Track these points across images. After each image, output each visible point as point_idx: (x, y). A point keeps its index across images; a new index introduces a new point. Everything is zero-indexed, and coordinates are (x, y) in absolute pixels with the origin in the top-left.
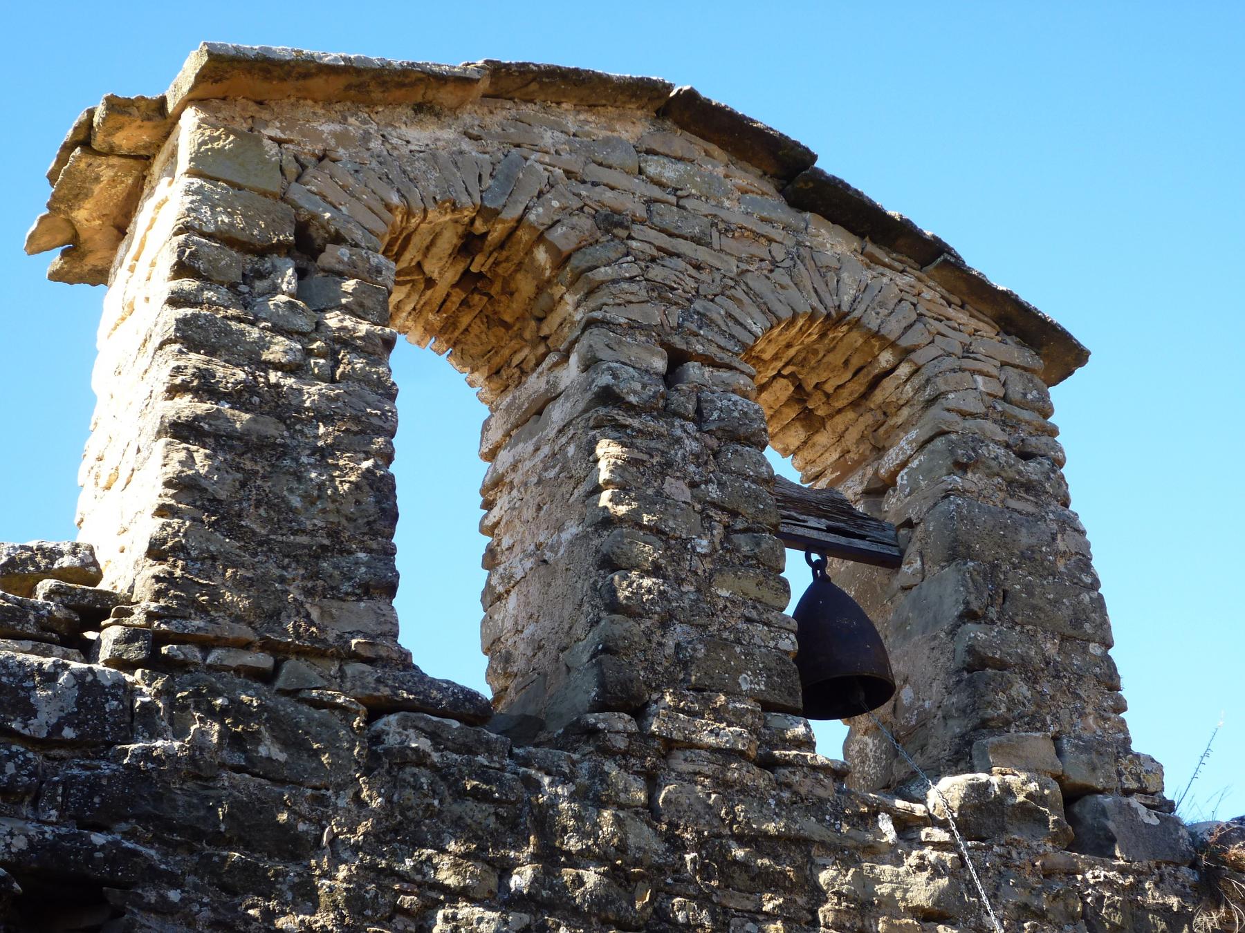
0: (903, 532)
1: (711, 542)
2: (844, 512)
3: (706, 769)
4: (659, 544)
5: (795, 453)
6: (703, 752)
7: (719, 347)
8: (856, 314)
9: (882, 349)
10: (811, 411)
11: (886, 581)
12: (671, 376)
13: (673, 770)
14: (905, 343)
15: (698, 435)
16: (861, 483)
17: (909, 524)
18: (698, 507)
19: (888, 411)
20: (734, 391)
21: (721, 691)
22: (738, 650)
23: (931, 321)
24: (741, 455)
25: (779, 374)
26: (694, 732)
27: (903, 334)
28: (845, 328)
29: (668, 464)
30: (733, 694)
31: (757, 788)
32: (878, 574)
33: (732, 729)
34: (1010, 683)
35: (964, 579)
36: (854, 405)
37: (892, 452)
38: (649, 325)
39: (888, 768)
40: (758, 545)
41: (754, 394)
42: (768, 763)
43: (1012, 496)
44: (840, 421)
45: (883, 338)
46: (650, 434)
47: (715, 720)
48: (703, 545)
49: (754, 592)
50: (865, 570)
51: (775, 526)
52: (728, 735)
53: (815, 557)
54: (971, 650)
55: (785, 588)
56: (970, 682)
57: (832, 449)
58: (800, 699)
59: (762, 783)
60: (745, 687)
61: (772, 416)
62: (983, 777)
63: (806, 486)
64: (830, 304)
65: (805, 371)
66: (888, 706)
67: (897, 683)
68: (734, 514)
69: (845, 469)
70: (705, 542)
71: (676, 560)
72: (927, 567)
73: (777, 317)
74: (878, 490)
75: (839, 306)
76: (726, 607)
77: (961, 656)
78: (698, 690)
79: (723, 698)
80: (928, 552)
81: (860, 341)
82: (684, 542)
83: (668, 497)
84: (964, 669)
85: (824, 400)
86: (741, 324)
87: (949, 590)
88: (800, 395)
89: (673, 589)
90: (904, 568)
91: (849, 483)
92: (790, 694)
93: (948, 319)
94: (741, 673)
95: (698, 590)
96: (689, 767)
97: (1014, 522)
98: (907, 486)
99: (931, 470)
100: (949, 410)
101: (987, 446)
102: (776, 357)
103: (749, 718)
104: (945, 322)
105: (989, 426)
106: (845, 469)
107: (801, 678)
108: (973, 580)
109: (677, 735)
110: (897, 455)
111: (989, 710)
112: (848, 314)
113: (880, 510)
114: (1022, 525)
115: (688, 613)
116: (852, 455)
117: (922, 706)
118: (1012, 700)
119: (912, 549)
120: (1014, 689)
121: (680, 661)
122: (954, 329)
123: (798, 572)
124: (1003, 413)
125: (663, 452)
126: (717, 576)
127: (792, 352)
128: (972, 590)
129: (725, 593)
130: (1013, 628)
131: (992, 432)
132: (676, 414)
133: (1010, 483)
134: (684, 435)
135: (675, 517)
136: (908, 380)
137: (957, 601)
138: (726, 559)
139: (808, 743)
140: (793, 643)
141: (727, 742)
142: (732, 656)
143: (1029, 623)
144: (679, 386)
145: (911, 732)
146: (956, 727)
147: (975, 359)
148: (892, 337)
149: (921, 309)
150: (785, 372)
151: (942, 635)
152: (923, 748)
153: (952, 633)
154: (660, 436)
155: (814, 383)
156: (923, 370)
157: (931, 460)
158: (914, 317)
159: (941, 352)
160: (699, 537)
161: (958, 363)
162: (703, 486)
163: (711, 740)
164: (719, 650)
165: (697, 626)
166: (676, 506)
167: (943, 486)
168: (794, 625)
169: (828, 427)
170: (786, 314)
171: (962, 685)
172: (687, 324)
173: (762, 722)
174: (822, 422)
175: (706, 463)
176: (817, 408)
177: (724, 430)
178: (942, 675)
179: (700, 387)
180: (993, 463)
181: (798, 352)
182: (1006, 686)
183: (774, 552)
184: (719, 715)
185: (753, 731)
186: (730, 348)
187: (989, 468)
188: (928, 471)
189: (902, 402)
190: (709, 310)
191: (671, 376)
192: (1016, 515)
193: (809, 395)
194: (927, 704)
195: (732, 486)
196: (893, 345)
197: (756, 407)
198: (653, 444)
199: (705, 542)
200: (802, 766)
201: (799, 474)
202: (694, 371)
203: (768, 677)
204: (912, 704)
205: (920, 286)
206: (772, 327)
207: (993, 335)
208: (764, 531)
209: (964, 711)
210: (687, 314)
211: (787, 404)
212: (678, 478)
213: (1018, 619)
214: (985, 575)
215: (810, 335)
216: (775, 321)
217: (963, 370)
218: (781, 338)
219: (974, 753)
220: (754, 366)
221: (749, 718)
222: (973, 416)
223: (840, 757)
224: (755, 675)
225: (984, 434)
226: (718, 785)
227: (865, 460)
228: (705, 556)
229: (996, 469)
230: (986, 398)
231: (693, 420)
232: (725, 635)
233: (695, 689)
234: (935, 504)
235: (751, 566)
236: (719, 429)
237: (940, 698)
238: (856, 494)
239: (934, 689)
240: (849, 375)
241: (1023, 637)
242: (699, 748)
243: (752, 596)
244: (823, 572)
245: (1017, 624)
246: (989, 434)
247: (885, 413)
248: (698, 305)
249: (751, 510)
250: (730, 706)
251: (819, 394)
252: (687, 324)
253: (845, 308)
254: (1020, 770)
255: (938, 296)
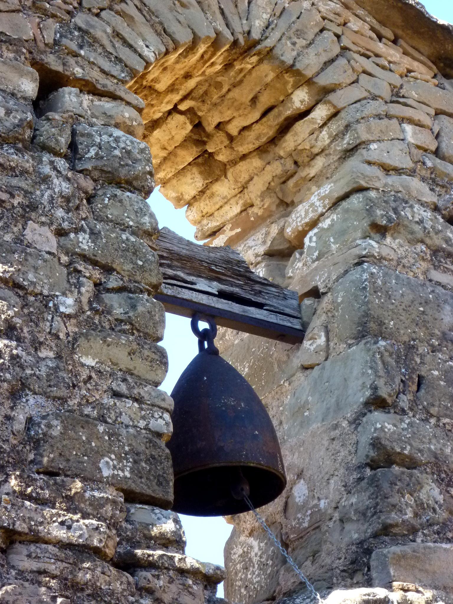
0: (307, 302)
1: (78, 301)
2: (239, 275)
3: (53, 568)
4: (15, 299)
5: (190, 204)
6: (50, 548)
7: (103, 71)
8: (268, 43)
9: (297, 86)
10: (211, 155)
11: (285, 358)
12: (42, 103)
13: (13, 567)
14: (323, 80)
15: (70, 174)
16: (264, 242)
17: (315, 293)
18: (65, 259)
19: (300, 160)
20: (117, 126)
21: (77, 476)
22: (101, 428)
23: (357, 56)
24: (121, 201)
25: (175, 109)
26: (41, 523)
27: (322, 70)
28: (255, 59)
29: (32, 207)
30: (92, 479)
31: (112, 593)
32: (276, 349)
33: (87, 521)
34: (420, 485)
35: (373, 360)
36: (261, 150)
37: (301, 209)
38: (20, 40)
39: (274, 576)
40: (134, 307)
41: (140, 131)
42: (127, 564)
43: (436, 268)
44: (243, 169)
45: (298, 73)
46: (13, 169)
47: (68, 510)
48: (67, 304)
49: (125, 362)
50: (261, 344)
51: (156, 287)
52: (83, 528)
53: (203, 325)
54: (376, 444)
55: (162, 360)
56: (373, 480)
57: (233, 201)
58: (171, 490)
59: (118, 587)
60: (106, 473)
61: (165, 159)
62: (380, 593)
63: (201, 243)
64: (238, 29)
65: (205, 108)
66: (278, 503)
67: (289, 477)
68: (108, 270)
69: (247, 225)
70: (70, 301)
71: (33, 320)
72: (332, 344)
73: (174, 41)
74: (282, 253)
75: (249, 33)
76: (90, 378)
77: (365, 451)
78: (51, 474)
79: (78, 485)
80: (334, 326)
81: (271, 76)
82: (45, 300)
83: (29, 246)
84: (367, 465)
85: (227, 142)
86: (130, 46)
87: (356, 371)
88: (199, 134)
89: (29, 354)
90: (306, 344)
91: (250, 243)
92: (160, 484)
93: (377, 55)
94: (103, 456)
95: (59, 357)
96: (34, 565)
97: (437, 298)
98: (316, 248)
99: (343, 232)
100: (369, 163)
101: (412, 207)
102: (172, 89)
103: (108, 510)
104: (374, 59)
105: (416, 184)
106: (247, 225)
107: (174, 465)
108: (383, 363)
109: (20, 526)
110: (307, 212)
111: (393, 515)
112: (258, 42)
113: (283, 276)
114: (445, 301)
115: (44, 383)
116: (255, 210)
117: (317, 506)
118: (420, 504)
119: (316, 324)
120: (424, 491)
121: (30, 438)
122: (383, 68)
123: (179, 342)
124: (433, 170)
125: (26, 192)
126: (82, 341)
127: (191, 83)
128: (381, 373)
129: (89, 361)
130: (426, 420)
131: (418, 191)
132: (45, 148)
133: (436, 251)
134: (53, 174)
135: (36, 269)
136: (325, 124)
137: (363, 385)
138: (94, 321)
139: (177, 542)
140: (167, 424)
141: (80, 536)
142: (94, 435)
143: (446, 416)
144: (51, 115)
145: (302, 535)
146: (355, 532)
147: (406, 105)
148: (309, 73)
149: (346, 42)
150: (183, 107)
151: (345, 424)
152: (315, 555)
153: (356, 422)
154: (24, 172)
155: (215, 123)
156: (342, 114)
157: (345, 220)
158: (337, 50)
159: (366, 94)
160: (64, 294)
161: (385, 108)
162: (72, 235)
163: (61, 534)
164: (78, 428)
165: (54, 398)
166: (38, 256)
167: (356, 251)
168: (170, 403)
169: (229, 175)
170: (184, 36)
171: (364, 484)
172: (65, 41)
173: (124, 515)
174: (224, 168)
175: (77, 208)
176: (218, 152)
177: (102, 171)
178: (342, 471)
179: (77, 117)
180: (417, 228)
181: (199, 84)
182: (414, 488)
183: (152, 317)
184: (72, 504)
185: (113, 525)
186: (115, 73)
187: (412, 233)
188: (341, 234)
189: (316, 150)
190: (92, 27)
191: (42, 103)
192: (439, 290)
193: (209, 136)
194: (322, 504)
195: (107, 237)
196: (309, 82)
197: (143, 145)
198: (15, 182)
199: (70, 301)
200: (167, 569)
201: (193, 229)
202: (70, 98)
203: (135, 462)
204: (306, 503)
205: (347, 14)
206: (167, 53)
207: (429, 77)
208: (141, 292)
209: (364, 514)
210: (66, 28)
211: (183, 145)
212: (43, 224)
213: (434, 410)
214: (399, 357)
215: (213, 64)
216: (171, 46)
217: (389, 117)
218: (178, 66)
219: (373, 563)
220: (145, 97)
221: (108, 510)
222: (398, 171)
223: (220, 562)
224: (120, 459)
225: (409, 193)
226: (66, 587)
227: (270, 216)
228: (69, 316)
229: (420, 235)
230: (415, 151)
231: (66, 157)
232: (87, 410)
233: (46, 473)
234: (346, 272)
235: (124, 332)
236: (95, 168)
237: (337, 497)
238: (257, 255)
239: (332, 486)
240: (257, 115)
241: (438, 432)
242: (46, 543)
243: (122, 367)
244: (211, 343)
245: (432, 416)
246: (414, 194)
247: (296, 163)
248: (80, 19)
249: (128, 267)
250: (87, 495)
251: (220, 137)
252: (65, 41)
253: (256, 35)
254: (425, 586)
255: (367, 27)
